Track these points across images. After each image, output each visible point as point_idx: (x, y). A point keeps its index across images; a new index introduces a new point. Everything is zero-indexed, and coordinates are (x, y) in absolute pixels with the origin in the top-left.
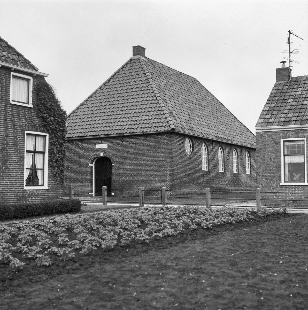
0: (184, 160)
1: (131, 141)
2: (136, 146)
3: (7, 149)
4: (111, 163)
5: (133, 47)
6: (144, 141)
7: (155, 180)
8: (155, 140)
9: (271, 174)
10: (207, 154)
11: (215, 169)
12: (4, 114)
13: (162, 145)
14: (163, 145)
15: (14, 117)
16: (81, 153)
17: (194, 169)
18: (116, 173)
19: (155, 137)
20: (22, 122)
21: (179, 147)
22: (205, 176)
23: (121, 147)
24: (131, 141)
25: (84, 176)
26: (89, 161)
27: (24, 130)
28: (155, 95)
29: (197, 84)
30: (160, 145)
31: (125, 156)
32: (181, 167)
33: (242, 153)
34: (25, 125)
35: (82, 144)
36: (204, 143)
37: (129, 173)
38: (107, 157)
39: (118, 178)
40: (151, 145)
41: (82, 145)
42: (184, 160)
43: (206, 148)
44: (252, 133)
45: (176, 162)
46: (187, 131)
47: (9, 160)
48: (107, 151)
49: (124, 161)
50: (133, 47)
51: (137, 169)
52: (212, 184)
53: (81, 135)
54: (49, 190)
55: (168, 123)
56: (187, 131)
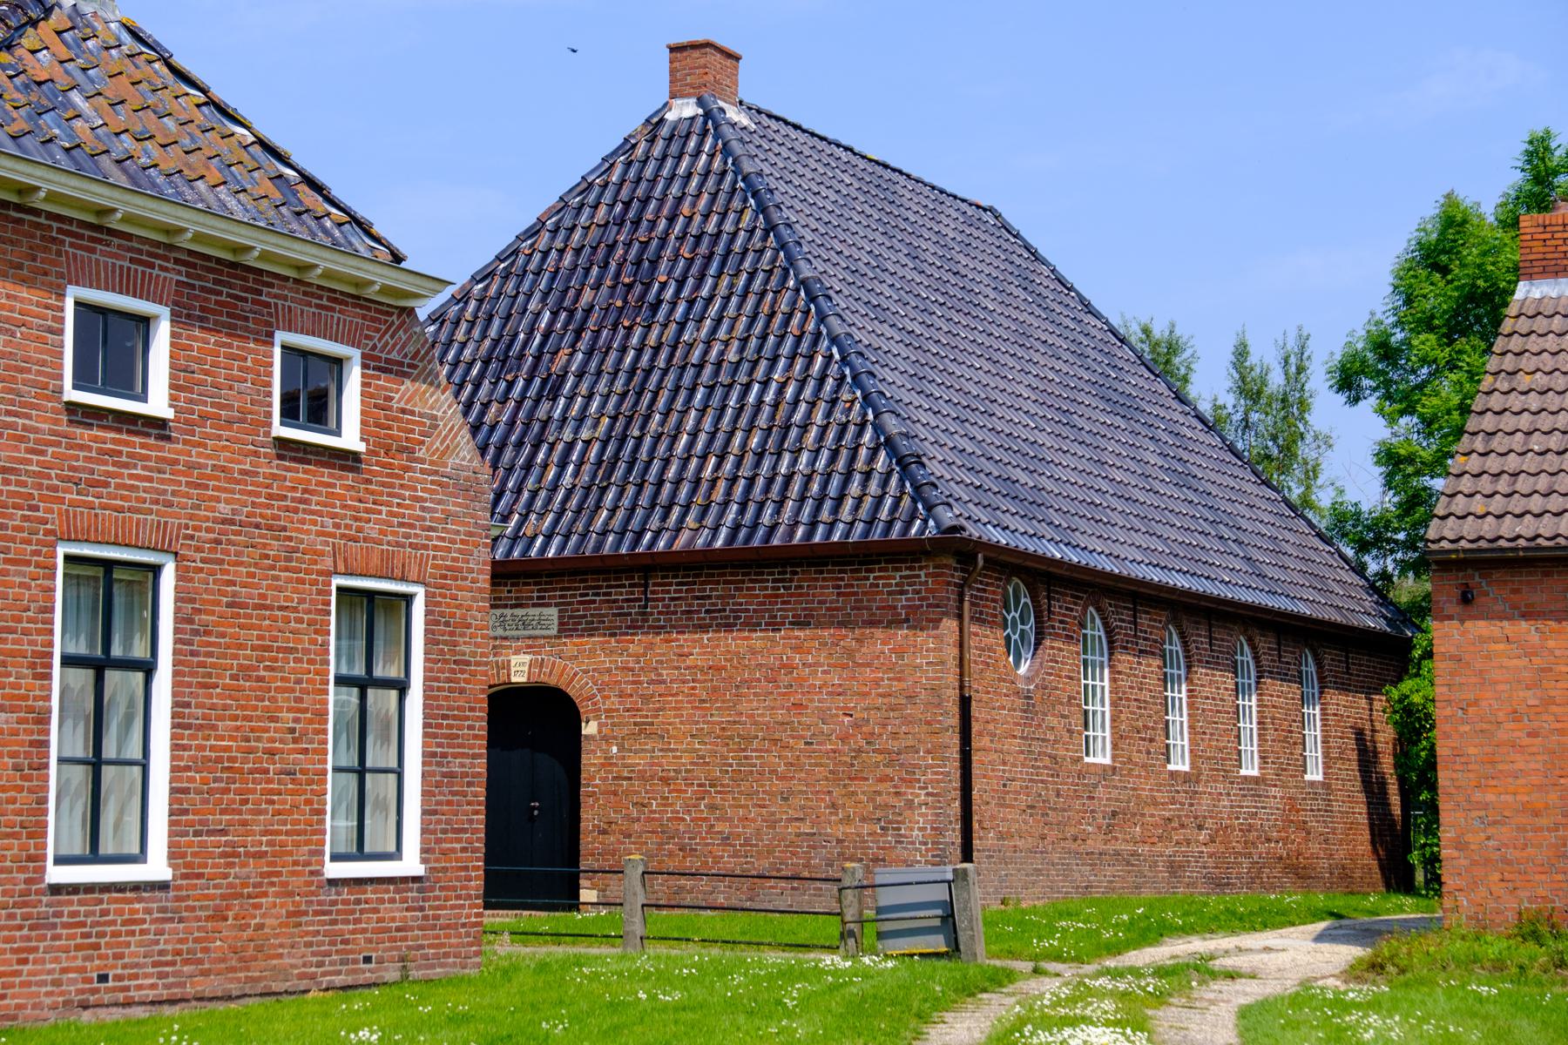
3: (262, 673)
5: (673, 49)
6: (777, 596)
8: (843, 594)
9: (1519, 798)
12: (250, 493)
15: (287, 509)
17: (1045, 754)
19: (842, 579)
20: (319, 534)
22: (1100, 792)
24: (698, 598)
27: (330, 574)
31: (664, 682)
33: (1280, 656)
34: (334, 544)
36: (1091, 609)
38: (552, 681)
43: (1102, 633)
44: (337, 192)
47: (267, 730)
49: (659, 709)
54: (428, 879)
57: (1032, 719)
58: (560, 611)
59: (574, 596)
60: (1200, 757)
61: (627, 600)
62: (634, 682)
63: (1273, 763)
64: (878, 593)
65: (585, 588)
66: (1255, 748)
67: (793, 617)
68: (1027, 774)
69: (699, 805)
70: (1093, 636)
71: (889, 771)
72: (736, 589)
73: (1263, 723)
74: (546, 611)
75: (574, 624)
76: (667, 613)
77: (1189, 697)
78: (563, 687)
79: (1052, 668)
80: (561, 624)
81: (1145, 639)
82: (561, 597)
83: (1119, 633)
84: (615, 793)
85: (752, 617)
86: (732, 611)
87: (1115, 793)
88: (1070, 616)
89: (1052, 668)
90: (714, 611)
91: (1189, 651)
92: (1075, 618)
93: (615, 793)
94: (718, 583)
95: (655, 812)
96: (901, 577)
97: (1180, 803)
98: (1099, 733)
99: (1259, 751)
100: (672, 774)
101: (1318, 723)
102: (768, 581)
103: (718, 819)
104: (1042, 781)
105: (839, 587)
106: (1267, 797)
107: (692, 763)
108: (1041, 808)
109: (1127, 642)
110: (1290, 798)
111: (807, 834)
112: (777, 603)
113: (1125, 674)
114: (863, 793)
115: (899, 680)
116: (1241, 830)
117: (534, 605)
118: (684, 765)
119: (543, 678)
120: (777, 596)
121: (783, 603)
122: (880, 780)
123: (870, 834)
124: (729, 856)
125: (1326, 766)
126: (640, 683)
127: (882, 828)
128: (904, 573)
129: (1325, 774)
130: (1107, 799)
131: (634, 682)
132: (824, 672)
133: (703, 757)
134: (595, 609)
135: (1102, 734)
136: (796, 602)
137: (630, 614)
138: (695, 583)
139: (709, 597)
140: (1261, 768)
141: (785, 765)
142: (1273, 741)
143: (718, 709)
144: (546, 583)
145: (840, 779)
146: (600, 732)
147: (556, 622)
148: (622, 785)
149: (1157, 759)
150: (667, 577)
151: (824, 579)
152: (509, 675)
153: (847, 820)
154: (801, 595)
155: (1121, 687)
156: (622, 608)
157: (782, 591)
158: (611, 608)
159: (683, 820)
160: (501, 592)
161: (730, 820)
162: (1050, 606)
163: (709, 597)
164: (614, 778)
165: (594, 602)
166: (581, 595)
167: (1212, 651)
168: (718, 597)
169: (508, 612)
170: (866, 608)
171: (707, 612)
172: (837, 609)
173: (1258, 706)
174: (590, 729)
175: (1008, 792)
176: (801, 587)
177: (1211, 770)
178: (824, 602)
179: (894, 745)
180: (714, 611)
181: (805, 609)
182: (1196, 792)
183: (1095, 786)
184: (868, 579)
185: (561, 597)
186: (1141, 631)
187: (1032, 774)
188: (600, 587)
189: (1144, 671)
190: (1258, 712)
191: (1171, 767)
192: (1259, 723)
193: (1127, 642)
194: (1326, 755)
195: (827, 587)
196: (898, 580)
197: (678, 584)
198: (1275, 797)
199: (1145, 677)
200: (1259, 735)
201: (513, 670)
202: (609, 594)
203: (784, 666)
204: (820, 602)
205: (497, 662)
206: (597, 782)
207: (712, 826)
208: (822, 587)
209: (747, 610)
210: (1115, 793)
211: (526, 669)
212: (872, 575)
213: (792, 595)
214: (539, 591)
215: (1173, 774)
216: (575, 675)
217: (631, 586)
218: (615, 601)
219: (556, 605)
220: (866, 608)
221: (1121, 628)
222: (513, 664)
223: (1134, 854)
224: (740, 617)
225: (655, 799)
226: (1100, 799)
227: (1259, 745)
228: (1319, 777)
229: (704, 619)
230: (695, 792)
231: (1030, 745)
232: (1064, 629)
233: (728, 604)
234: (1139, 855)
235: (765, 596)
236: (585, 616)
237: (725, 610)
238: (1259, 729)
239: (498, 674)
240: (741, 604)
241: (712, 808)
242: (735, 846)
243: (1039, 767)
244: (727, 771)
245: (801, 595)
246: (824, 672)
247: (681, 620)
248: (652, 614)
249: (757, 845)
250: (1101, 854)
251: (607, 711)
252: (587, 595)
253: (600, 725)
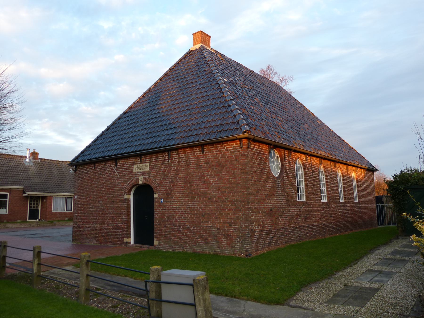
0: (269, 187)
1: (181, 158)
2: (188, 165)
4: (153, 194)
5: (193, 34)
6: (201, 156)
7: (218, 223)
10: (303, 174)
11: (316, 198)
13: (228, 161)
14: (231, 161)
16: (115, 179)
18: (159, 210)
19: (218, 149)
21: (260, 164)
22: (302, 209)
23: (168, 167)
24: (181, 158)
25: (119, 213)
26: (125, 190)
28: (219, 86)
29: (279, 104)
30: (226, 162)
31: (173, 182)
32: (263, 199)
35: (116, 166)
37: (178, 210)
38: (148, 183)
39: (162, 217)
40: (212, 162)
41: (117, 167)
42: (269, 187)
43: (302, 166)
45: (255, 189)
46: (270, 137)
48: (147, 175)
50: (193, 34)
51: (190, 203)
52: (313, 222)
53: (115, 153)
55: (238, 123)
56: (270, 137)
57: (280, 190)
58: (150, 164)
59: (152, 160)
60: (330, 198)
61: (165, 160)
62: (166, 183)
63: (347, 198)
64: (227, 152)
65: (155, 157)
66: (343, 195)
67: (205, 161)
68: (279, 206)
69: (182, 217)
70: (299, 167)
71: (232, 207)
72: (190, 154)
73: (345, 189)
74: (146, 164)
75: (153, 167)
76: (174, 163)
77: (326, 183)
78: (150, 185)
79: (286, 175)
80: (150, 167)
81: (314, 168)
82: (150, 160)
83: (307, 166)
84: (162, 213)
85: (194, 162)
86: (189, 161)
87: (307, 209)
88: (292, 161)
89: (286, 175)
90: (185, 161)
91: (326, 171)
92: (293, 161)
93: (162, 213)
94: (186, 153)
95: (171, 219)
96: (234, 147)
97: (325, 210)
98: (302, 193)
99: (344, 196)
100: (175, 208)
101: (356, 189)
102: (198, 151)
103: (186, 222)
104: (284, 208)
105: (217, 151)
106: (347, 207)
107: (180, 205)
108: (284, 216)
109: (309, 168)
110: (351, 207)
111: (209, 226)
112: (200, 158)
113: (309, 177)
114: (224, 214)
115: (234, 178)
116: (341, 216)
117: (144, 163)
118: (178, 206)
119: (146, 182)
120: (201, 156)
121: (202, 157)
122: (229, 210)
123: (226, 227)
124: (189, 233)
125: (359, 198)
126: (168, 182)
127: (230, 225)
128: (235, 146)
129: (358, 200)
130: (305, 211)
131: (166, 183)
132: (213, 177)
133: (182, 203)
134: (157, 163)
135: (303, 193)
136: (206, 157)
137: (165, 164)
138: (180, 154)
139: (184, 157)
140: (344, 200)
141: (203, 206)
142: (347, 193)
143: (186, 189)
144: (147, 157)
145: (218, 210)
146: (158, 196)
147: (149, 167)
148: (163, 212)
149: (319, 199)
150: (173, 153)
151: (213, 150)
152: (139, 182)
153: (220, 223)
154: (207, 155)
155: (308, 180)
156: (163, 162)
157: (202, 154)
158: (161, 162)
159: (178, 221)
160: (137, 160)
161: (189, 222)
162: (285, 157)
163: (184, 157)
164: (162, 210)
165: (157, 161)
166: (154, 159)
167: (331, 171)
168: (186, 157)
169: (138, 165)
170: (224, 157)
171: (183, 161)
172: (216, 158)
173: (343, 185)
174: (156, 196)
175: (272, 212)
176: (207, 152)
177: (332, 201)
178: (213, 156)
179: (232, 199)
180: (185, 161)
181: (208, 159)
182: (329, 207)
183: (301, 208)
184: (225, 148)
185: (150, 160)
186: (313, 166)
187: (280, 206)
188: (158, 157)
189: (314, 176)
190: (343, 186)
191: (322, 201)
192: (343, 189)
193: (309, 168)
194: (359, 196)
195: (214, 152)
196: (233, 148)
197: (176, 154)
198: (348, 207)
199: (314, 178)
200: (344, 192)
201: (139, 180)
202: (160, 159)
203: (202, 176)
204: (212, 156)
205: (136, 178)
206: (158, 211)
207: (185, 224)
208: (212, 152)
209: (193, 160)
210: (307, 209)
211: (142, 180)
212: (226, 147)
213: (204, 155)
214: (145, 159)
215: (323, 203)
216: (153, 181)
217: (166, 156)
218: (162, 160)
219: (149, 162)
220: (224, 157)
221: (307, 164)
222: (139, 179)
223: (313, 225)
224: (191, 163)
225: (171, 215)
226: (303, 211)
227: (344, 194)
228: (357, 201)
229: (182, 164)
230: (181, 214)
231: (280, 197)
232: (290, 164)
233: (188, 159)
234: (315, 225)
235: (198, 156)
236: (155, 165)
237: (187, 161)
238: (344, 190)
239: (136, 181)
240: (191, 159)
241: (185, 218)
242: (191, 229)
243: (283, 204)
244: (188, 208)
245: (207, 155)
246: (213, 177)
247: (177, 164)
248: (170, 163)
249: (196, 230)
250: (303, 227)
251: (160, 191)
252: (155, 159)
253: (158, 195)
